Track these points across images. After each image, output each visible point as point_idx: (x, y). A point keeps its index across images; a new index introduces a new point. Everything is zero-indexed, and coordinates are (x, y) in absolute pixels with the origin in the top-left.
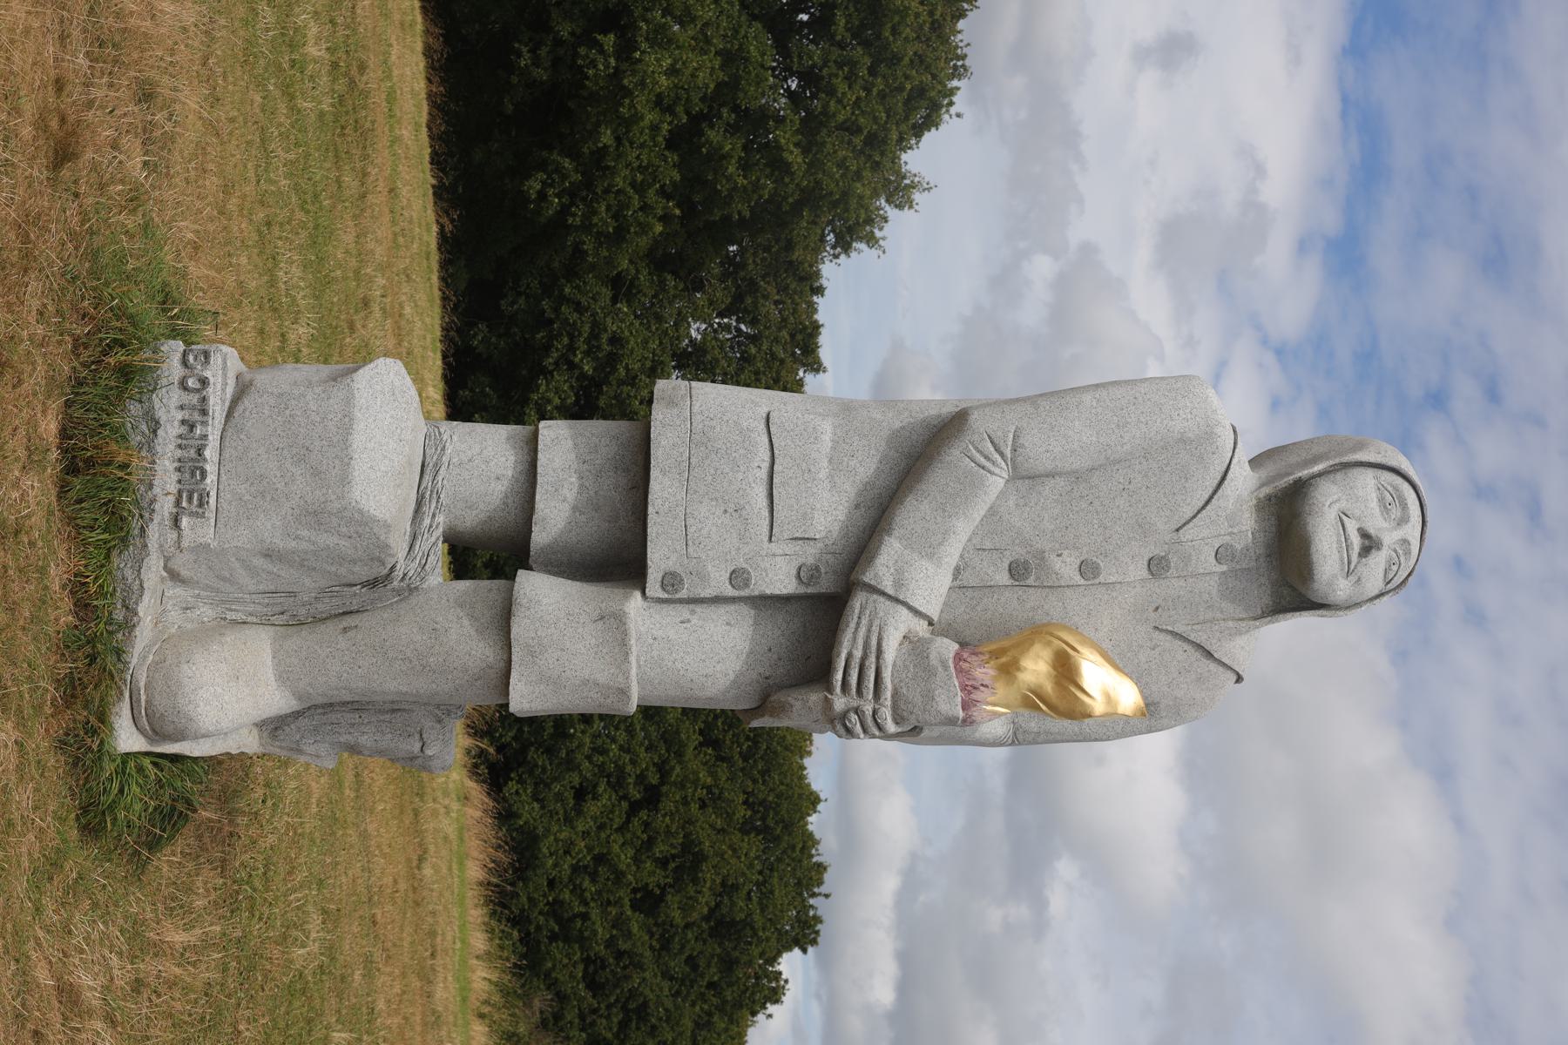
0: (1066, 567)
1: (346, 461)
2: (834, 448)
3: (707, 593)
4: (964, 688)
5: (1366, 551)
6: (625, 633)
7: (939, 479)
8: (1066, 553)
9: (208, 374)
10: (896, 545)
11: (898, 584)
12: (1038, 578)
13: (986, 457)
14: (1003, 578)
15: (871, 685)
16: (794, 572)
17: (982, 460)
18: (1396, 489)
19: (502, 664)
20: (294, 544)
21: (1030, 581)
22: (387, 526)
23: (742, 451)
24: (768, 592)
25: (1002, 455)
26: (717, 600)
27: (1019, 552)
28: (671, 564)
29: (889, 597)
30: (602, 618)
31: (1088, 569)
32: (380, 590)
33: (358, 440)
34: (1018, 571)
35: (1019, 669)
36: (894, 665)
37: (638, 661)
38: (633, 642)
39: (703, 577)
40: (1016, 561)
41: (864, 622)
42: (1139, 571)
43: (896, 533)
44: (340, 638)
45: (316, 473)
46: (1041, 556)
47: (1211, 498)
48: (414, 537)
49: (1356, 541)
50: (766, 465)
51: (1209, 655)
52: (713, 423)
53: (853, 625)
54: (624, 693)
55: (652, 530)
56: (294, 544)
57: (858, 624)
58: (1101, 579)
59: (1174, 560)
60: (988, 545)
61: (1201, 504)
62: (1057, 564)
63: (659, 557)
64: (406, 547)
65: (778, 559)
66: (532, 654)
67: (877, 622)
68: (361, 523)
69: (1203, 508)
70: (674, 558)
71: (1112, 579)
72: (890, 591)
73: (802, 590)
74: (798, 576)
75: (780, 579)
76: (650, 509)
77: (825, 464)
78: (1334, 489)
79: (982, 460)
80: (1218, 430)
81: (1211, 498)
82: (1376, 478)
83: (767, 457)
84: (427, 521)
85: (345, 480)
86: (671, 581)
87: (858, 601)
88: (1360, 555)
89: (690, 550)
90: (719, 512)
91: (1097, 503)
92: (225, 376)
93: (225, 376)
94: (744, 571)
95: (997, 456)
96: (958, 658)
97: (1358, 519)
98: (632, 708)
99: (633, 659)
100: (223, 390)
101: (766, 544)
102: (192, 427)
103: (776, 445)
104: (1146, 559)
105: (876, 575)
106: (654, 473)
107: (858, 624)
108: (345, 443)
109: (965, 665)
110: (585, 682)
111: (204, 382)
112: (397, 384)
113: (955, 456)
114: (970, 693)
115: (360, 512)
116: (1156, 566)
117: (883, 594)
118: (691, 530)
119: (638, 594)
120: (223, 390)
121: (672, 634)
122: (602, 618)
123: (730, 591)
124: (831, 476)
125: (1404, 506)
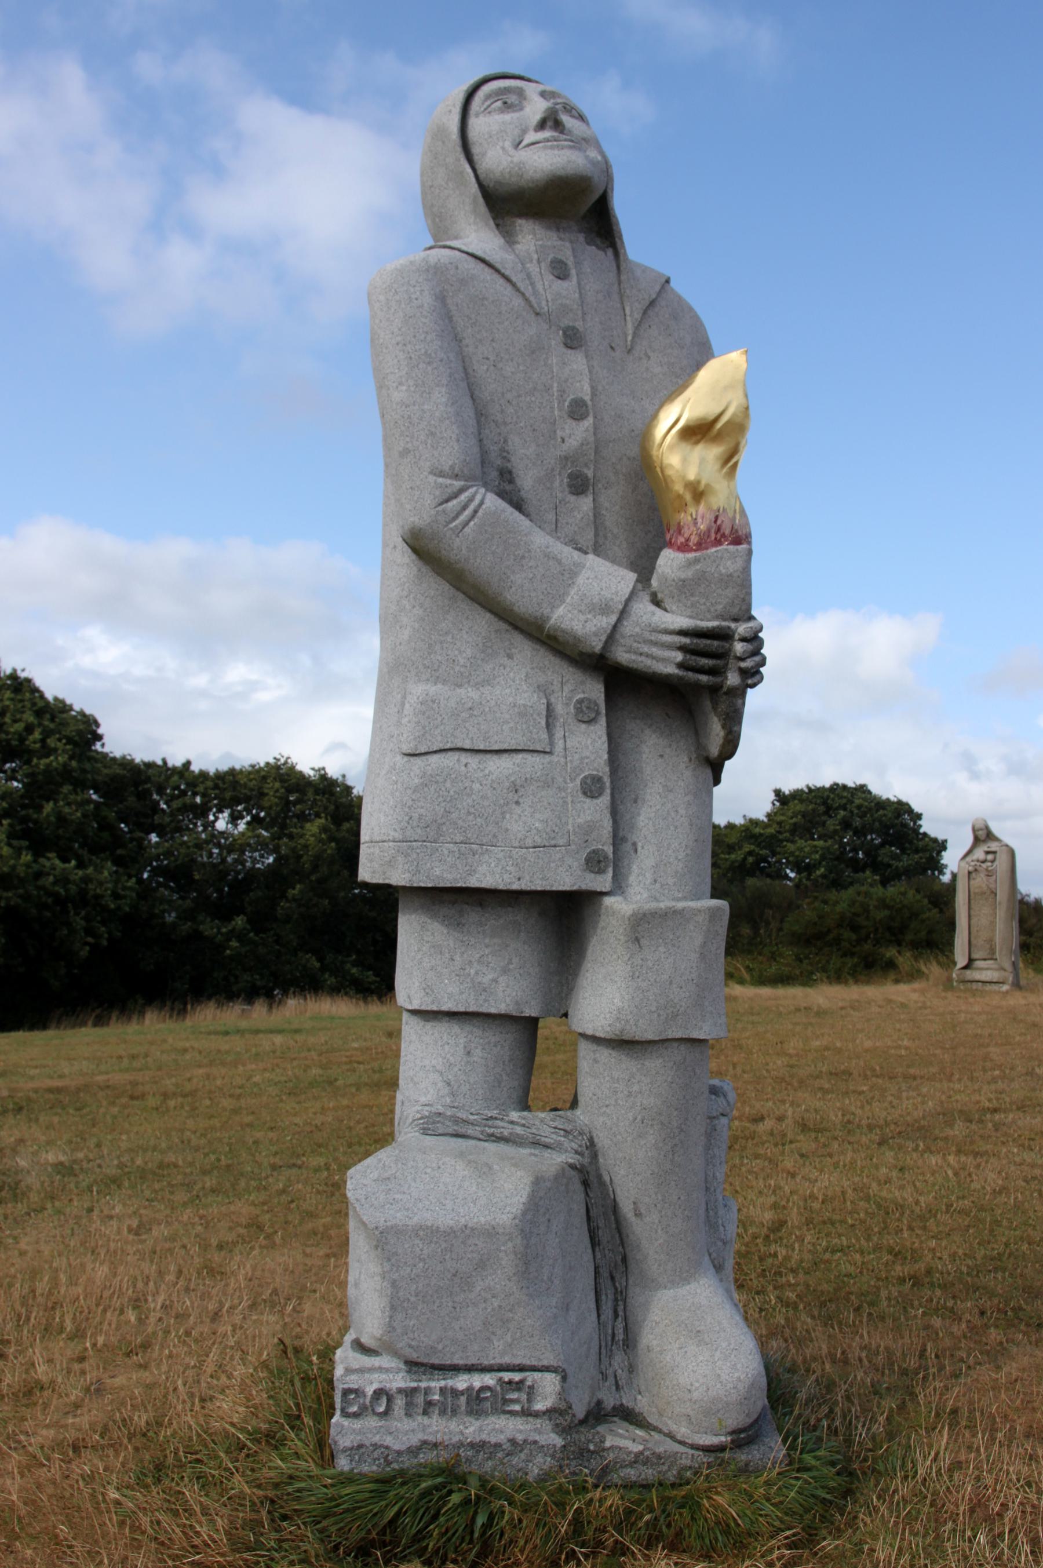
0: (576, 434)
1: (465, 1233)
2: (445, 682)
3: (607, 824)
4: (718, 542)
5: (558, 125)
6: (654, 914)
7: (482, 565)
8: (559, 433)
9: (370, 1391)
10: (561, 611)
11: (604, 609)
12: (586, 465)
13: (464, 508)
14: (586, 503)
15: (716, 643)
16: (583, 726)
17: (468, 512)
18: (488, 97)
19: (682, 1047)
20: (557, 1282)
21: (590, 474)
22: (537, 1181)
23: (448, 785)
24: (606, 756)
25: (462, 490)
26: (615, 812)
27: (561, 483)
28: (577, 863)
29: (619, 620)
30: (637, 940)
31: (578, 410)
32: (592, 1178)
33: (445, 1220)
34: (579, 485)
35: (699, 482)
36: (690, 617)
37: (679, 900)
38: (662, 905)
39: (588, 829)
40: (570, 486)
41: (645, 649)
42: (577, 361)
43: (546, 611)
44: (647, 1219)
45: (481, 1265)
46: (565, 459)
47: (503, 276)
48: (536, 1144)
49: (547, 134)
50: (464, 758)
51: (652, 303)
52: (416, 816)
53: (649, 662)
54: (713, 913)
55: (539, 885)
56: (557, 1282)
57: (647, 656)
58: (587, 398)
59: (566, 322)
60: (551, 516)
61: (509, 288)
62: (573, 443)
63: (565, 876)
64: (547, 1153)
65: (569, 744)
66: (675, 1016)
67: (647, 635)
68: (535, 1209)
69: (514, 285)
70: (569, 861)
71: (587, 388)
72: (613, 619)
73: (603, 721)
74: (589, 722)
75: (588, 745)
76: (515, 887)
77: (461, 691)
78: (491, 153)
79: (468, 512)
80: (432, 261)
81: (503, 276)
82: (477, 115)
83: (454, 756)
84: (519, 1130)
85: (490, 1233)
86: (595, 862)
87: (622, 656)
88: (562, 132)
89: (561, 842)
90: (518, 810)
91: (509, 396)
92: (372, 1370)
93: (372, 1370)
94: (584, 782)
95: (463, 497)
96: (684, 548)
97: (524, 132)
98: (723, 904)
99: (680, 905)
100: (387, 1370)
101: (554, 758)
102: (429, 1404)
103: (441, 746)
104: (564, 350)
105: (596, 634)
106: (473, 882)
107: (647, 656)
108: (450, 1233)
109: (694, 539)
110: (703, 956)
111: (378, 1393)
112: (375, 1175)
113: (459, 546)
114: (723, 535)
115: (524, 1213)
116: (573, 339)
117: (615, 627)
118: (539, 841)
119: (608, 901)
120: (387, 1370)
121: (650, 862)
122: (637, 940)
123: (605, 799)
124: (477, 686)
125: (507, 90)
